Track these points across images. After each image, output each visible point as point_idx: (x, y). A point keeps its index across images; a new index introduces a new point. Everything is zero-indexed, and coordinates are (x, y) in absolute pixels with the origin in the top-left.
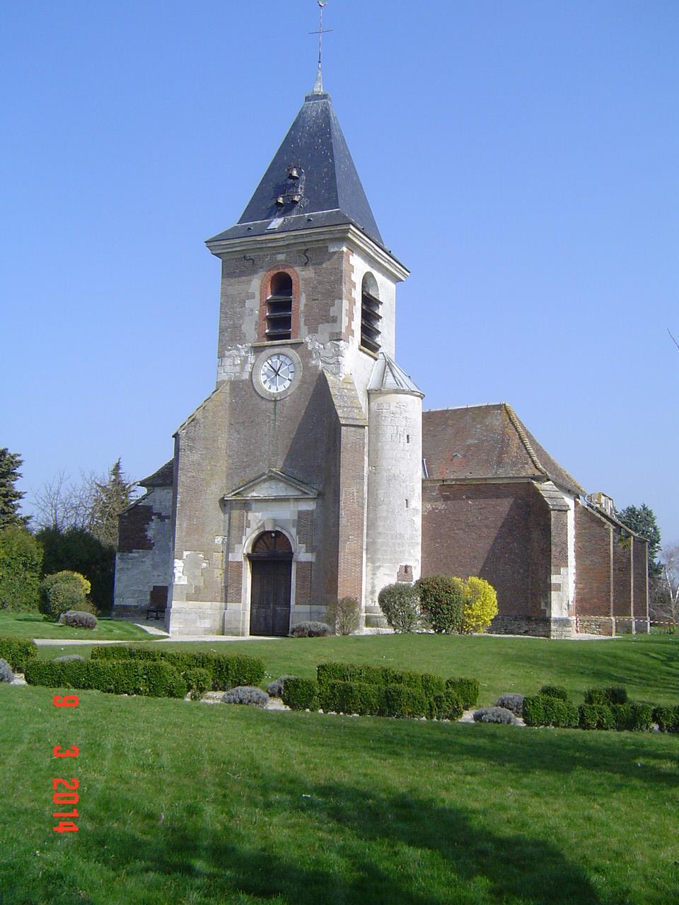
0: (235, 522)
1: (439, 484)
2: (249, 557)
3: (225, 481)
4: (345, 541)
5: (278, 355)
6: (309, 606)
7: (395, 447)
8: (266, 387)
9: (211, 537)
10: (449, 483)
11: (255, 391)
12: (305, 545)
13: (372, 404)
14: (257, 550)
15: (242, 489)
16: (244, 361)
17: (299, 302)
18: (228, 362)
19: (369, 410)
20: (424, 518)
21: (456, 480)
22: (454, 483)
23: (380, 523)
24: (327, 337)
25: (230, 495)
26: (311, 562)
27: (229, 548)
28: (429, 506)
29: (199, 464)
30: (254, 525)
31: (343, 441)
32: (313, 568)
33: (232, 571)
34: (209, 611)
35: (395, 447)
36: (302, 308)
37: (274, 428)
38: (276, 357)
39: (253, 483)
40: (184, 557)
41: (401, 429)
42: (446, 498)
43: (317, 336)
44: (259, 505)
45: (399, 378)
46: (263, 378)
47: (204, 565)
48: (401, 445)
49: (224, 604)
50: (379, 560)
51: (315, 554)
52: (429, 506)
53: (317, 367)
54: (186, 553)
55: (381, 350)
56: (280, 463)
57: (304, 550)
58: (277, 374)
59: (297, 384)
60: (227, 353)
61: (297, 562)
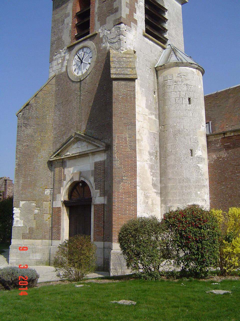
0: (57, 178)
1: (221, 138)
2: (65, 203)
3: (52, 148)
4: (119, 182)
5: (83, 48)
6: (102, 243)
7: (178, 108)
8: (75, 73)
9: (41, 190)
10: (228, 135)
11: (69, 78)
12: (99, 190)
13: (160, 78)
14: (72, 197)
15: (59, 151)
16: (63, 59)
17: (94, 7)
18: (55, 63)
19: (158, 83)
20: (210, 166)
21: (234, 131)
22: (232, 134)
23: (170, 171)
24: (112, 24)
25: (53, 157)
26: (104, 204)
27: (54, 198)
28: (214, 156)
29: (32, 136)
30: (68, 178)
31: (115, 93)
32: (105, 209)
33: (56, 213)
34: (40, 247)
35: (178, 108)
36: (96, 10)
37: (80, 102)
38: (82, 50)
39: (65, 146)
40: (21, 205)
41: (183, 93)
42: (227, 148)
43: (106, 26)
44: (72, 162)
45: (181, 57)
46: (74, 68)
47: (36, 211)
48: (184, 105)
49: (51, 241)
50: (170, 201)
51: (106, 197)
52: (214, 156)
53: (105, 48)
54: (22, 203)
55: (169, 42)
56: (84, 128)
57: (98, 194)
58: (82, 62)
59: (93, 64)
60: (54, 58)
61: (95, 205)
